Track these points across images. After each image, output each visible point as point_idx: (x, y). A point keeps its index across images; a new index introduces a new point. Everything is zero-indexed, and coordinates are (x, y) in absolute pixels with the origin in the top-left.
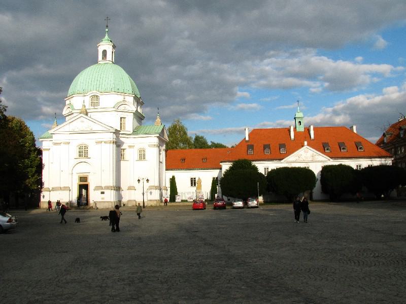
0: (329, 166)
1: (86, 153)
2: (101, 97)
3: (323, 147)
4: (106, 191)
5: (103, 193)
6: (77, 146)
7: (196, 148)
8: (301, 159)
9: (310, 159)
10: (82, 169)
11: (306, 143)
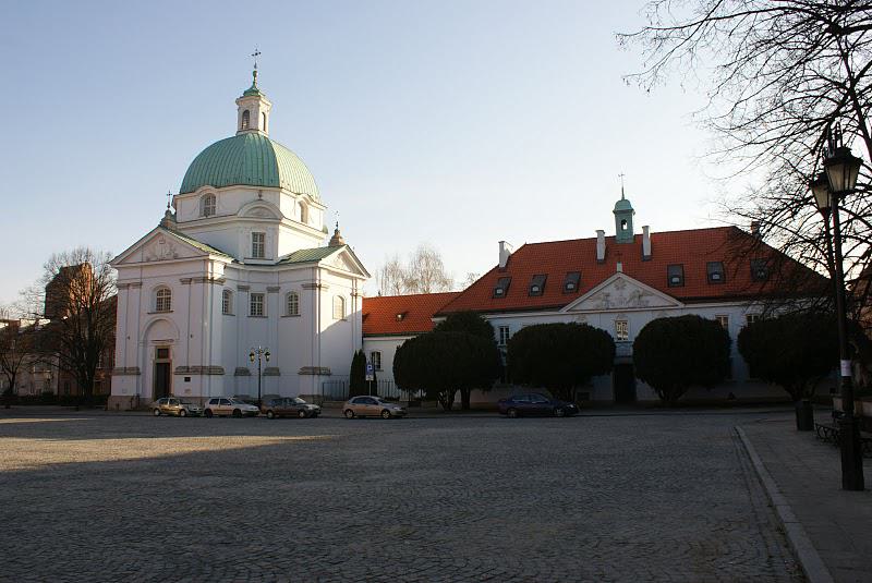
4: (192, 377)
5: (187, 380)
6: (155, 290)
10: (161, 334)
11: (619, 267)
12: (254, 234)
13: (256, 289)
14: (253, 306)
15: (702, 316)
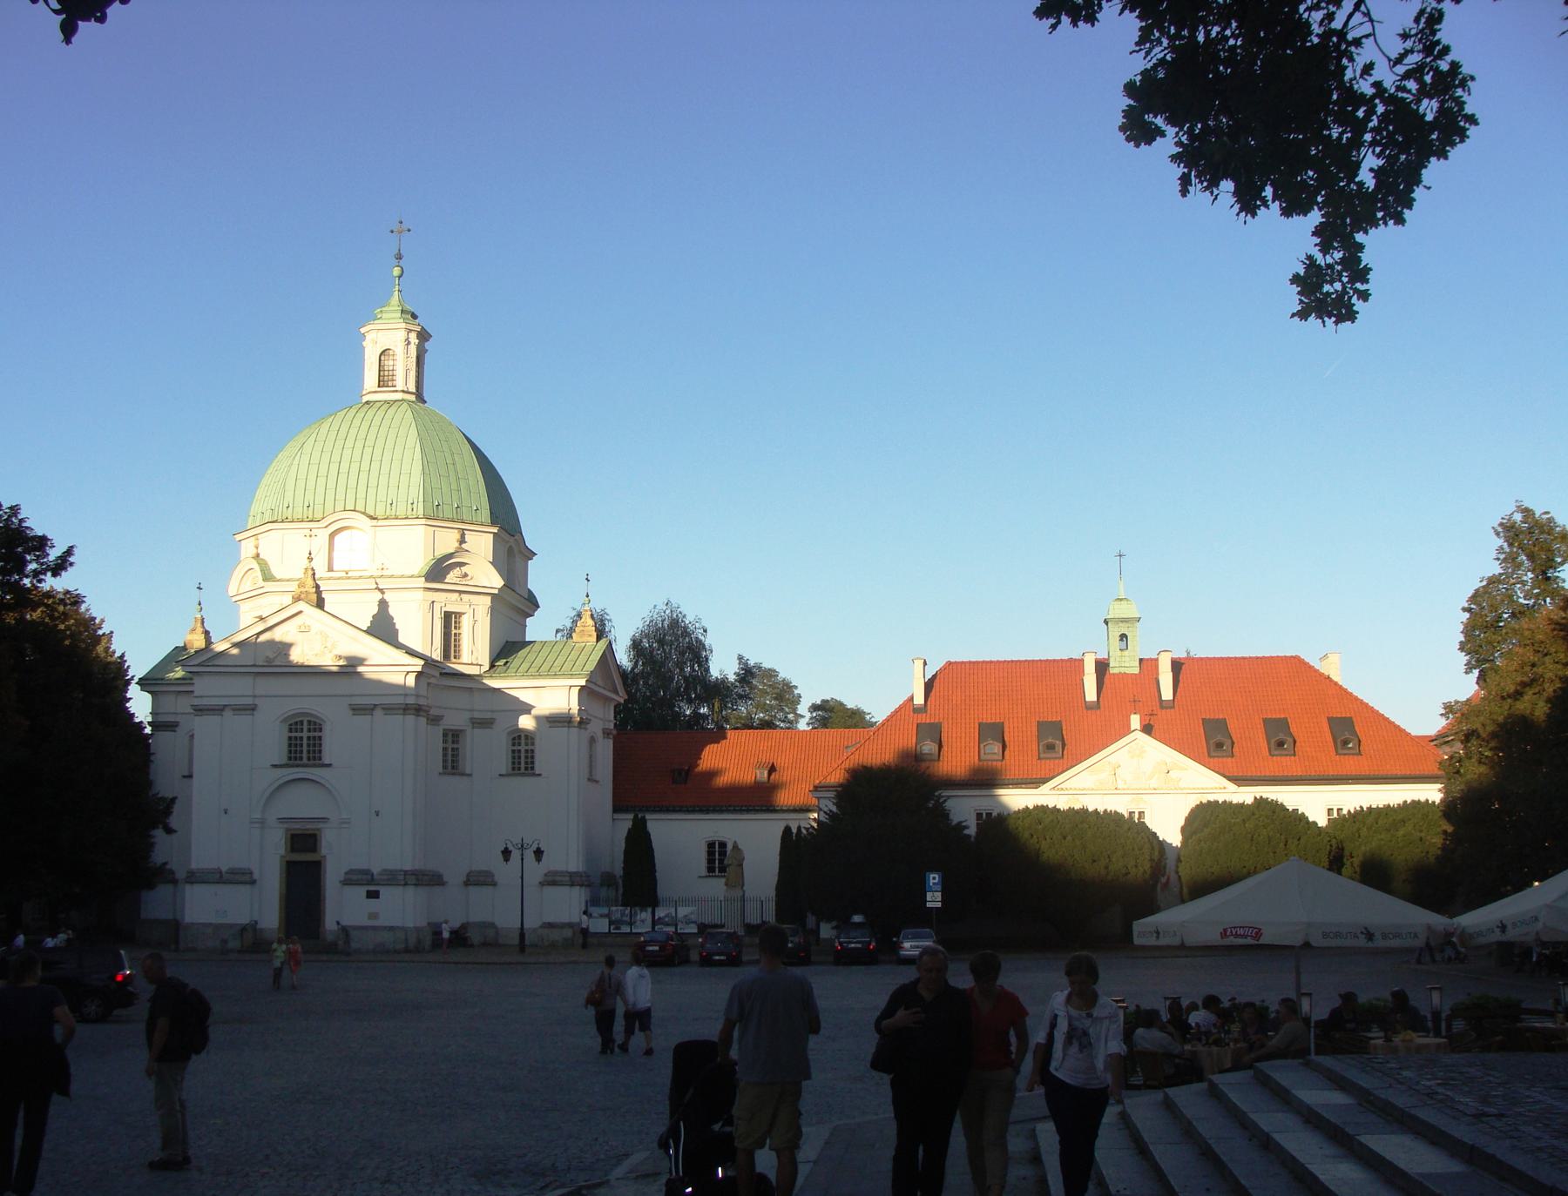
1: (531, 755)
3: (1214, 744)
4: (383, 890)
5: (373, 895)
6: (284, 720)
10: (302, 804)
13: (454, 720)
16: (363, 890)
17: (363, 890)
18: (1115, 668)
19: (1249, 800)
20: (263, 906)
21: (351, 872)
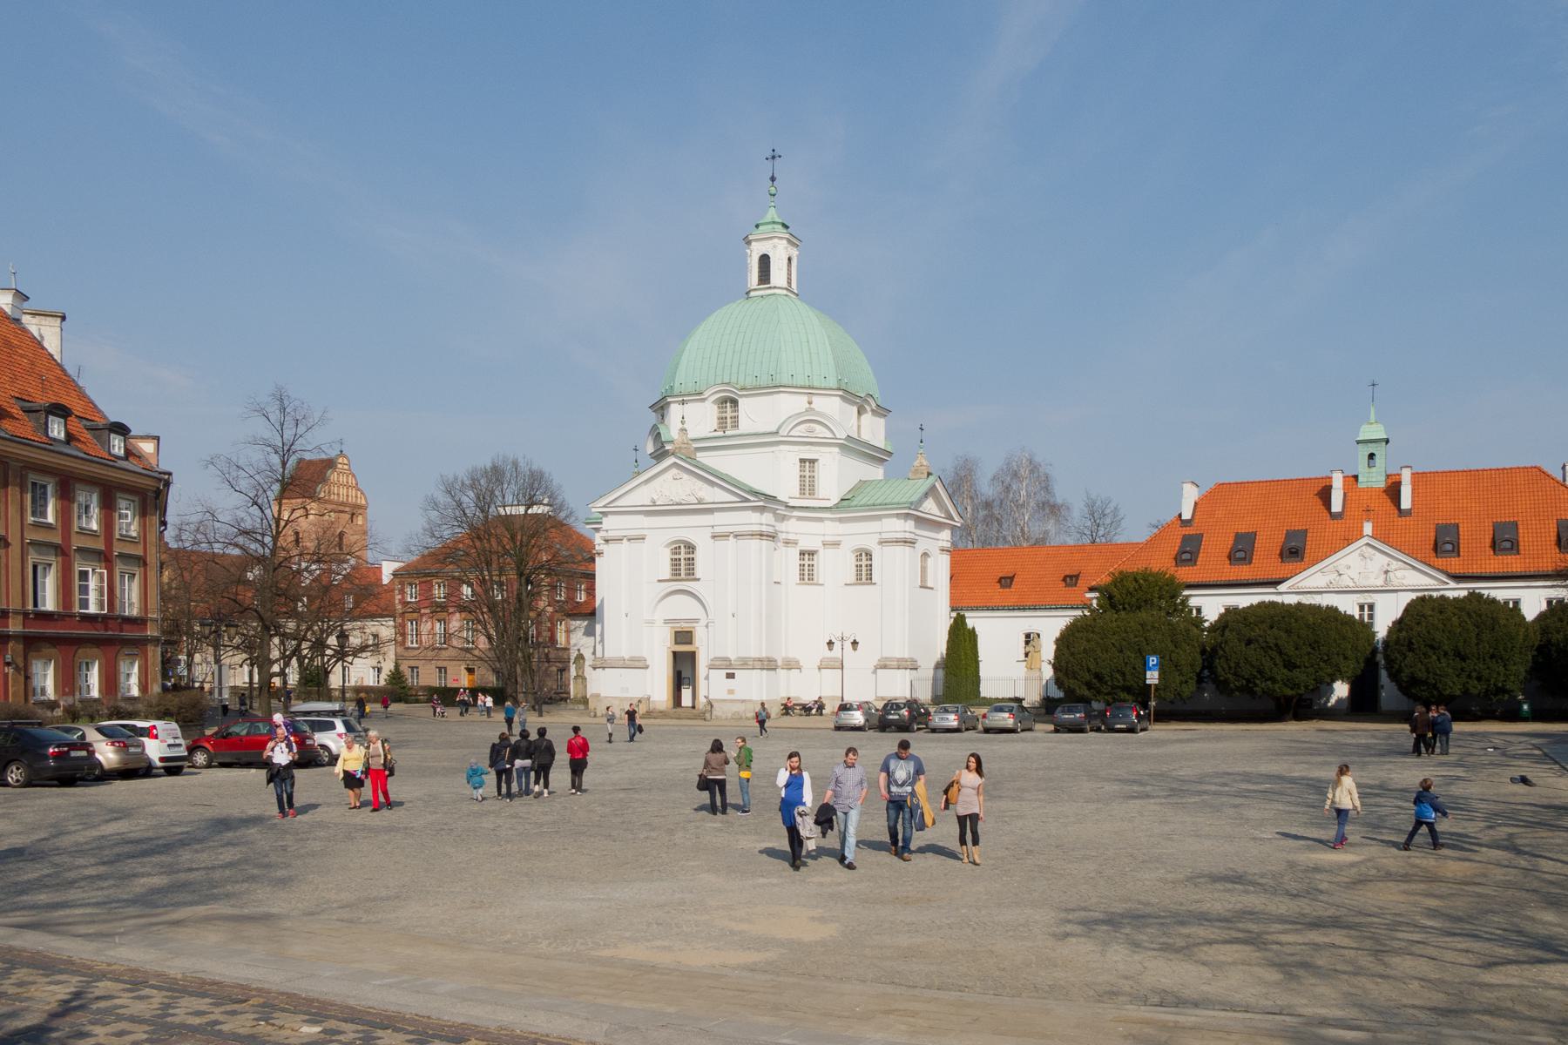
0: (1315, 609)
1: (691, 562)
2: (741, 401)
3: (1442, 545)
5: (730, 676)
7: (676, 655)
8: (1346, 582)
9: (1370, 583)
10: (683, 608)
11: (1368, 528)
12: (802, 461)
14: (675, 563)
15: (1342, 609)
16: (724, 672)
17: (724, 672)
18: (1363, 482)
19: (1464, 593)
20: (655, 686)
21: (716, 659)
